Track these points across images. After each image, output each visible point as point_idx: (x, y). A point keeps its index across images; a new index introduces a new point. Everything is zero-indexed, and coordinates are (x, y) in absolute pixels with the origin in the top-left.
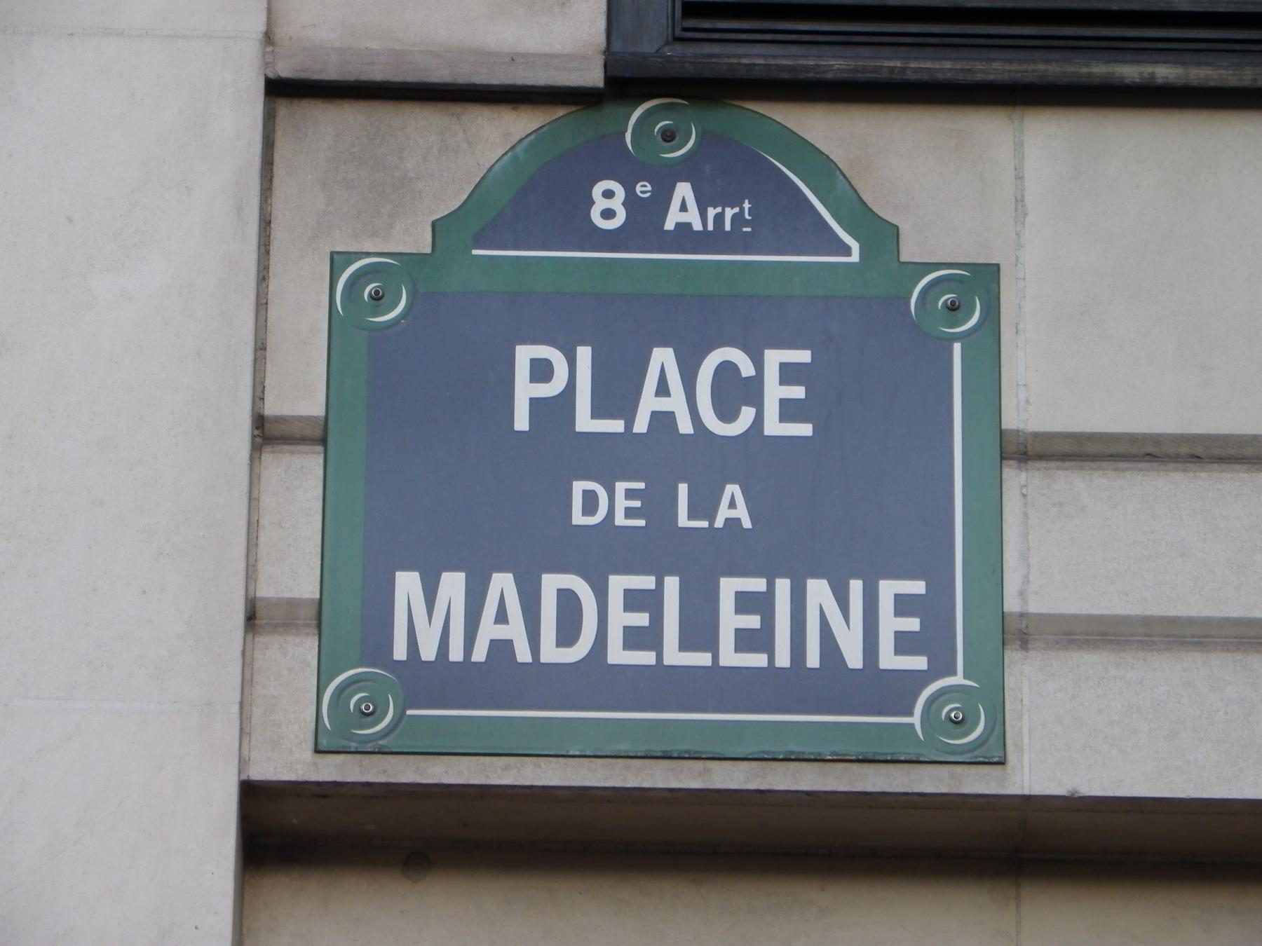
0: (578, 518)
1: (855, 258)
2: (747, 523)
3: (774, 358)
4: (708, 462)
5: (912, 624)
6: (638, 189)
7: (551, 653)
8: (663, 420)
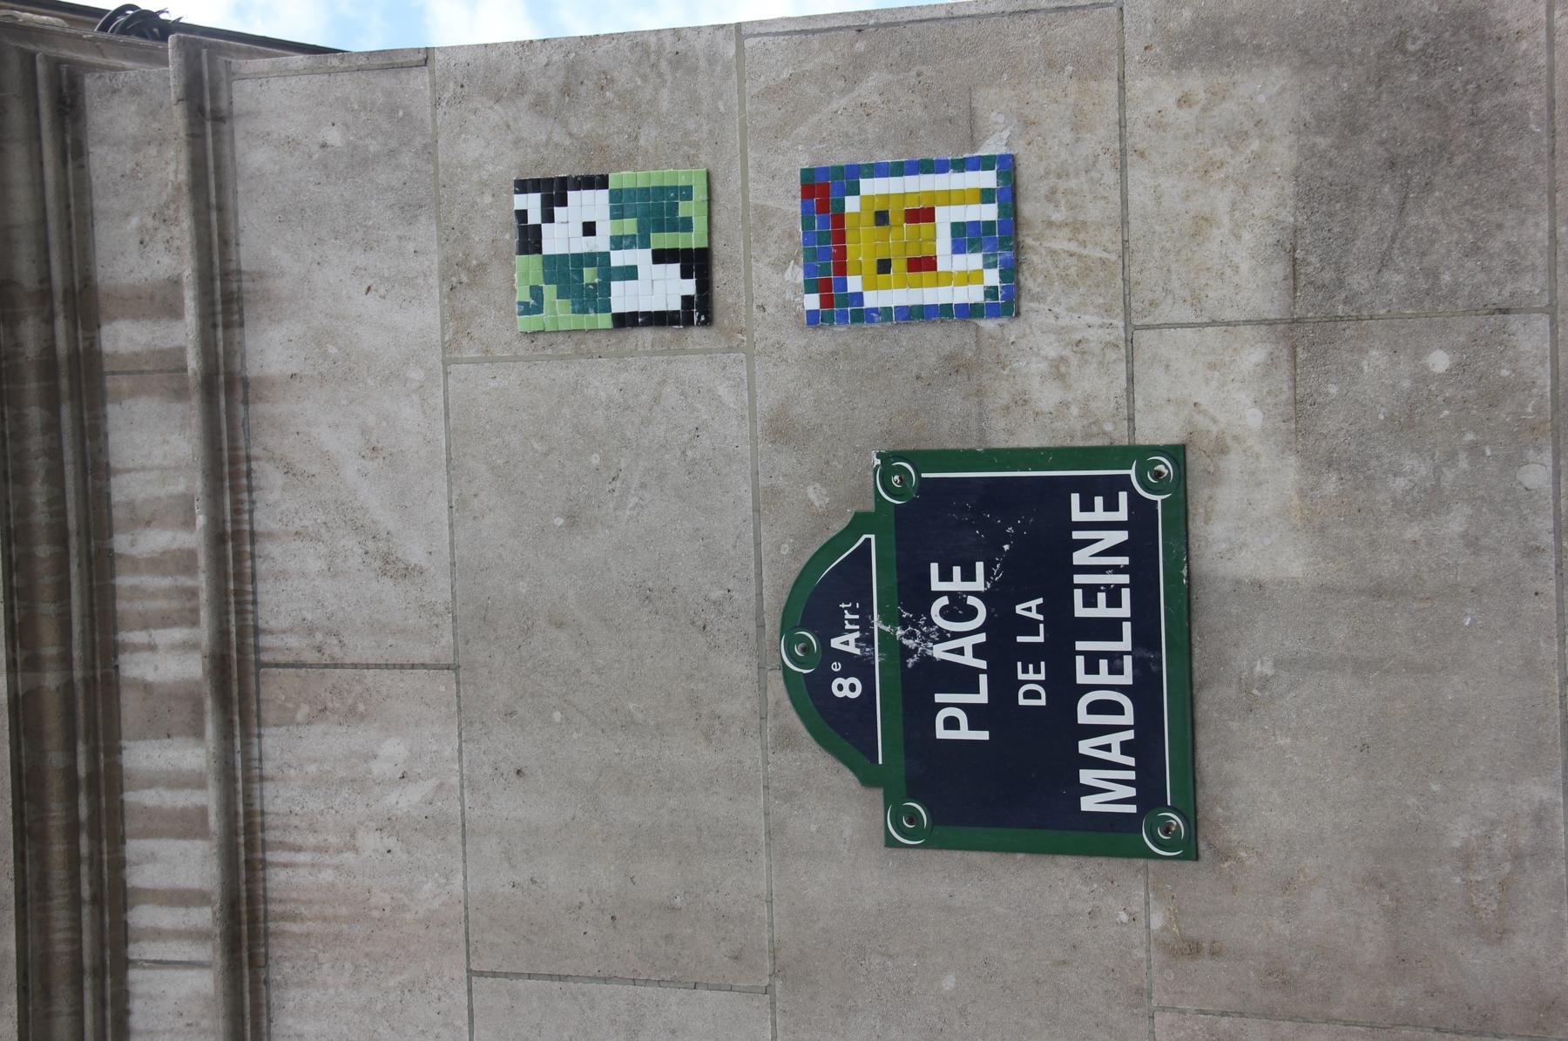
0: (1042, 702)
4: (1002, 627)
7: (1128, 718)
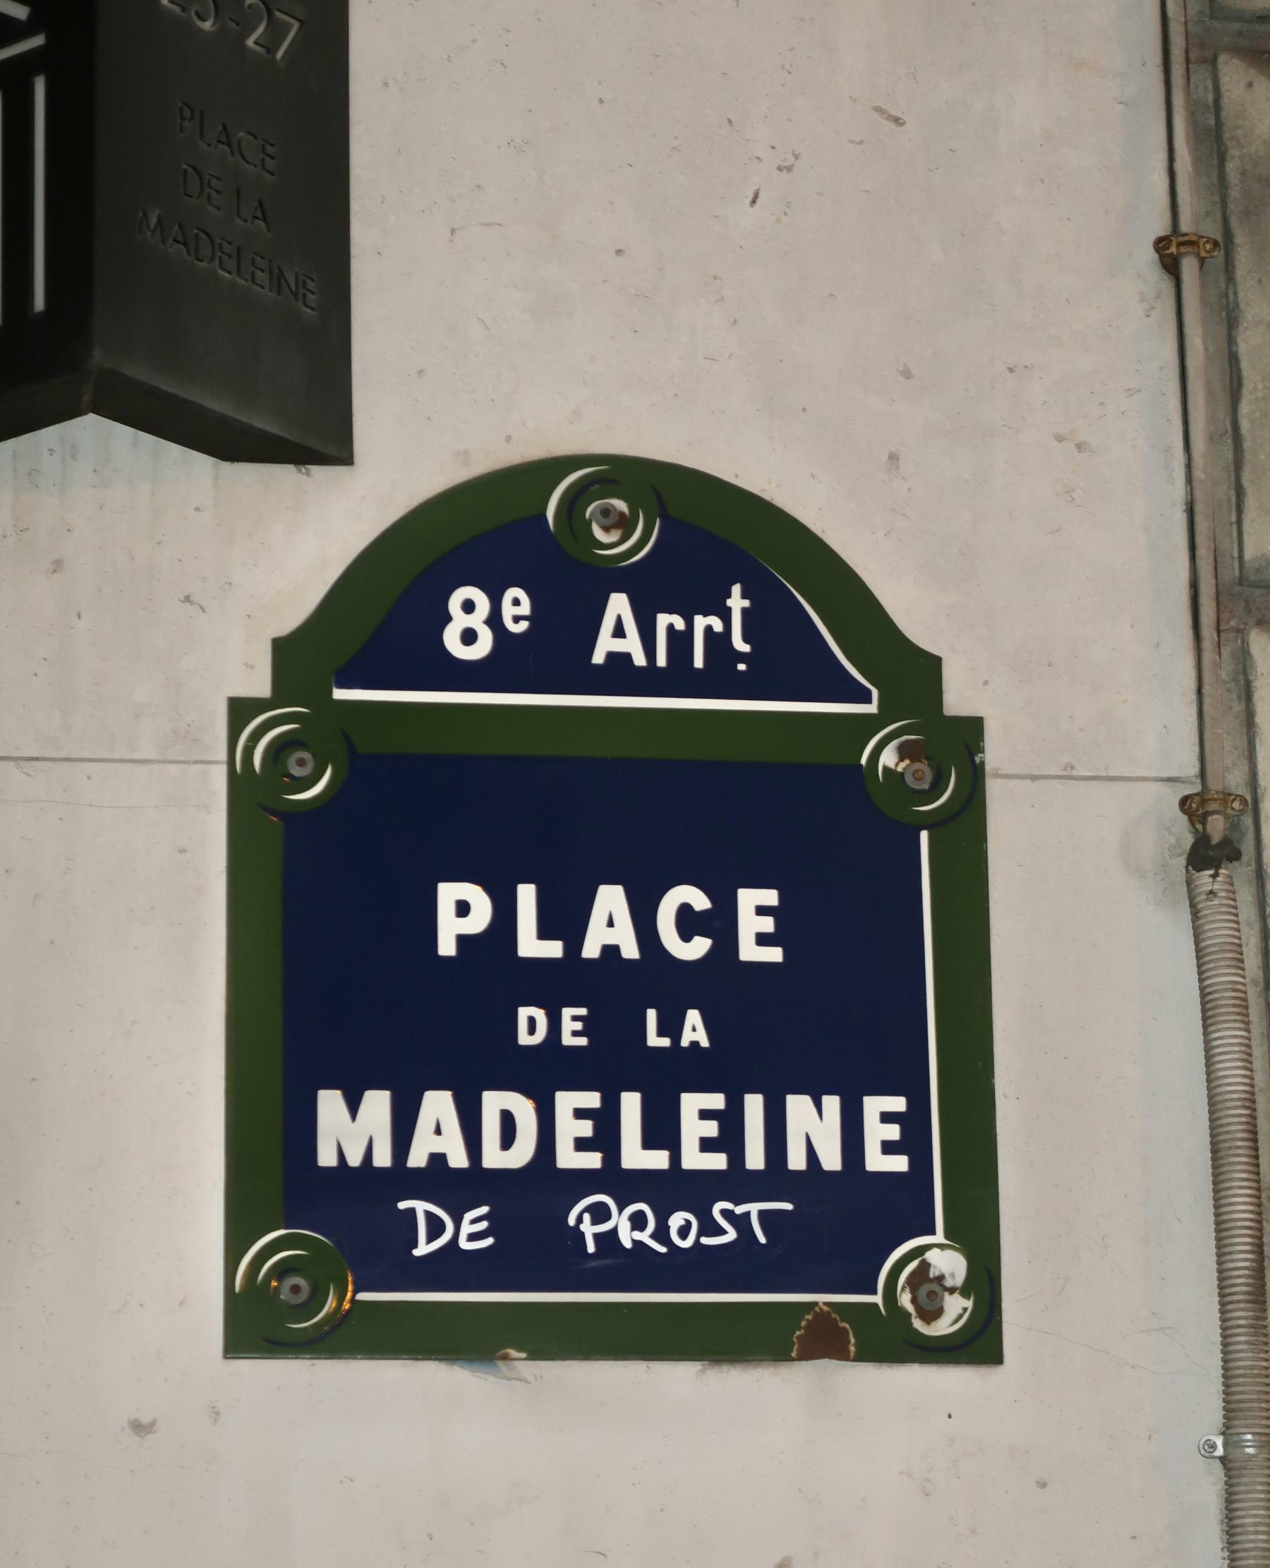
2: (705, 1043)
4: (655, 978)
7: (493, 1157)
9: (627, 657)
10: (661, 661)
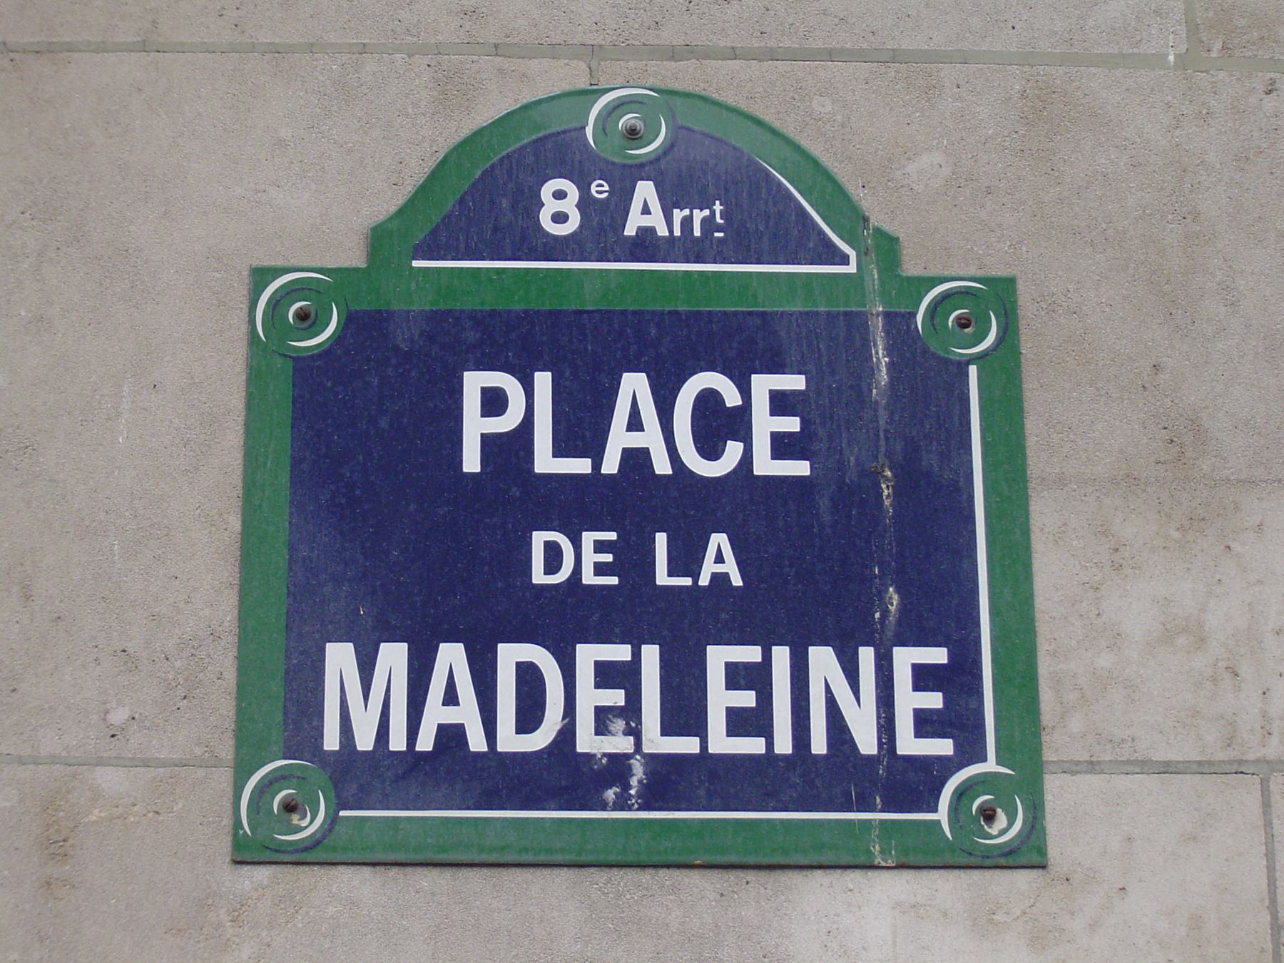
0: (539, 576)
1: (852, 268)
2: (737, 581)
3: (763, 384)
4: (689, 507)
5: (934, 700)
6: (593, 188)
7: (510, 741)
8: (636, 459)
9: (652, 230)
10: (677, 233)
